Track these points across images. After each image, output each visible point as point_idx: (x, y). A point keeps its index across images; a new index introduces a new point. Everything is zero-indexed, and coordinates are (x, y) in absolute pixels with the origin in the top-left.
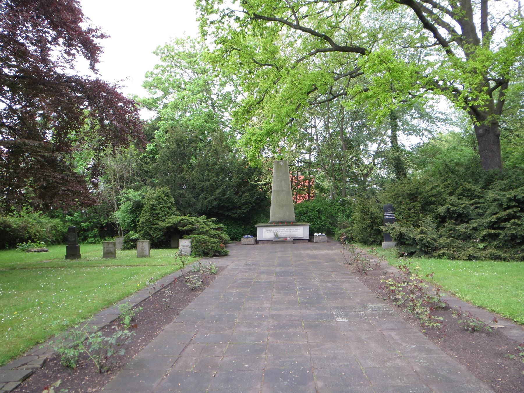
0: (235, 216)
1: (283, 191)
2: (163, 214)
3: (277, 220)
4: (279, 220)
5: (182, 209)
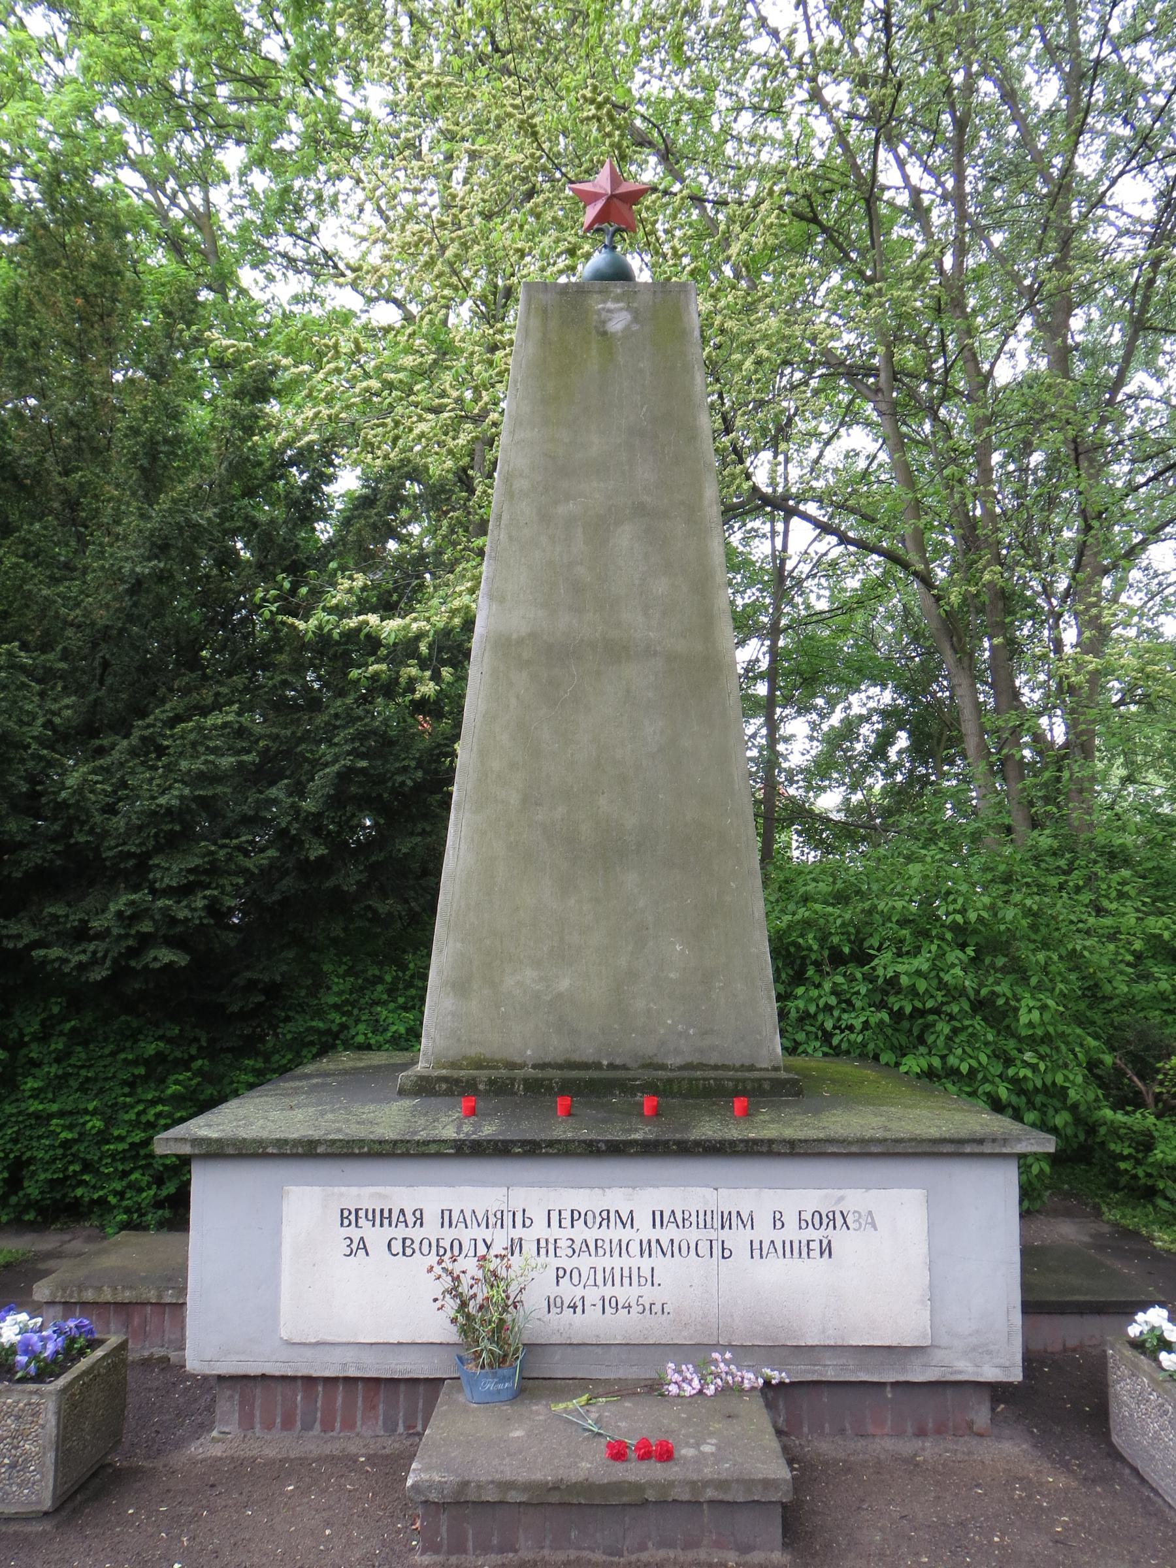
1: (616, 651)
3: (524, 1042)
4: (557, 1048)
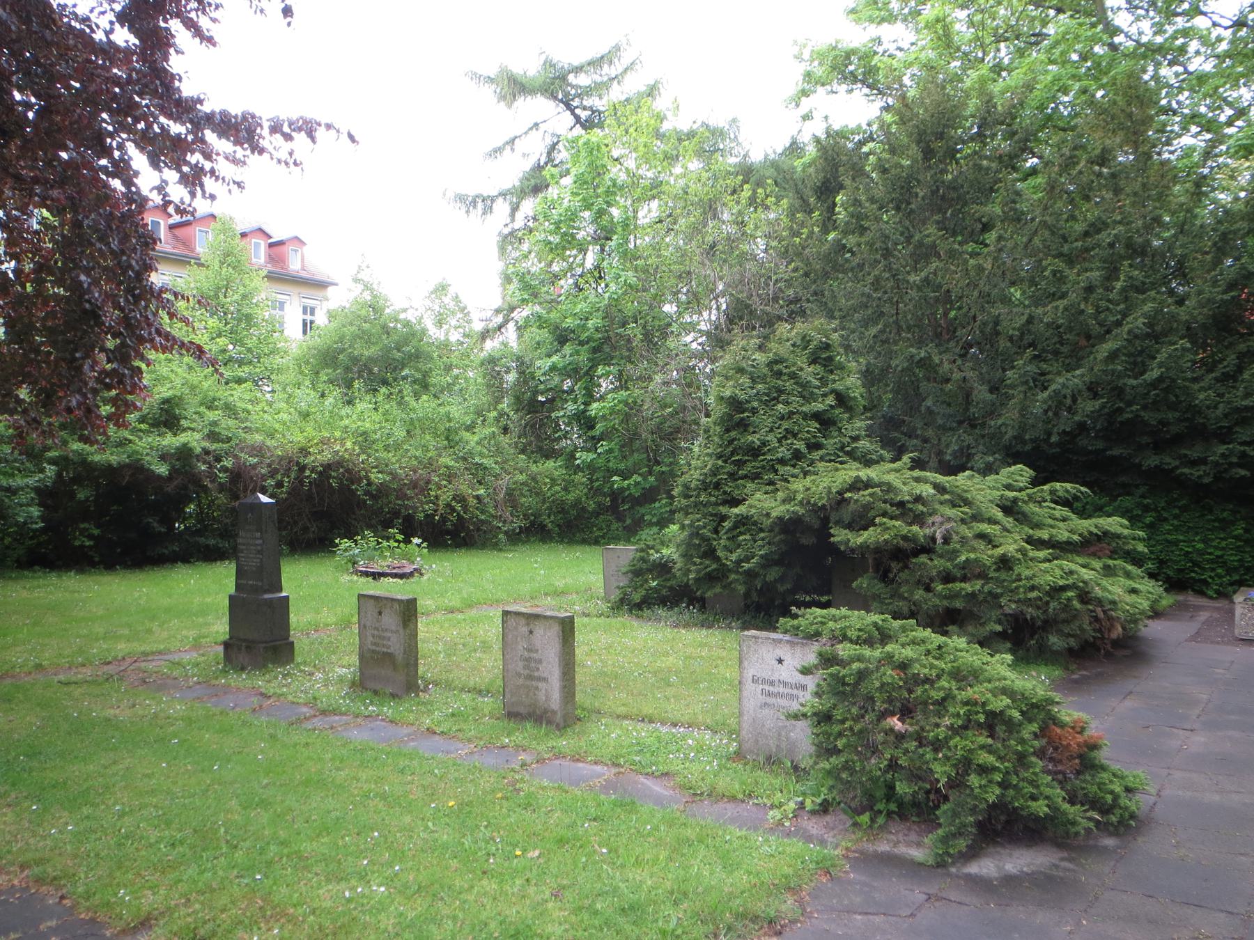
0: (1196, 473)
2: (783, 452)
5: (930, 433)
